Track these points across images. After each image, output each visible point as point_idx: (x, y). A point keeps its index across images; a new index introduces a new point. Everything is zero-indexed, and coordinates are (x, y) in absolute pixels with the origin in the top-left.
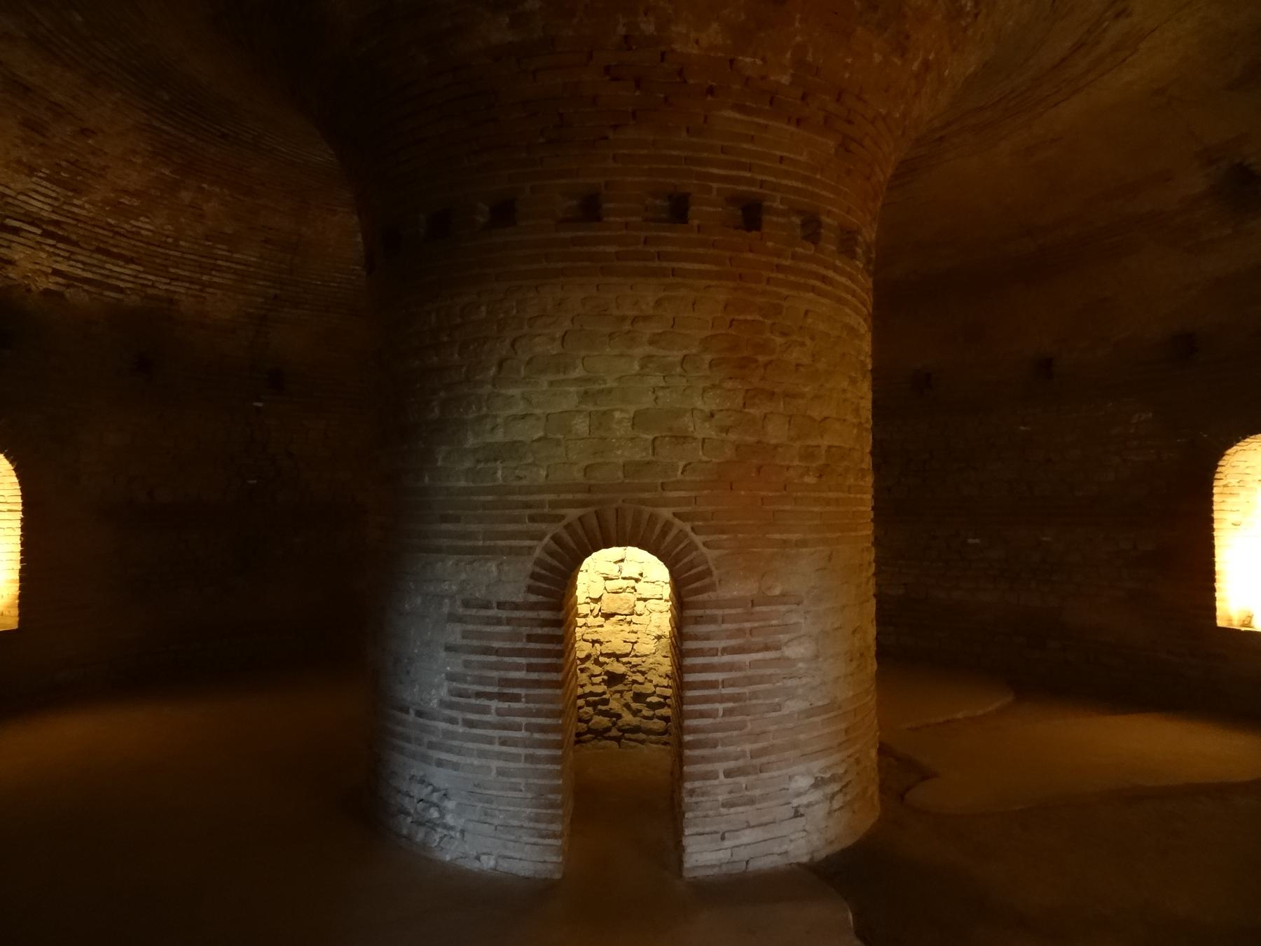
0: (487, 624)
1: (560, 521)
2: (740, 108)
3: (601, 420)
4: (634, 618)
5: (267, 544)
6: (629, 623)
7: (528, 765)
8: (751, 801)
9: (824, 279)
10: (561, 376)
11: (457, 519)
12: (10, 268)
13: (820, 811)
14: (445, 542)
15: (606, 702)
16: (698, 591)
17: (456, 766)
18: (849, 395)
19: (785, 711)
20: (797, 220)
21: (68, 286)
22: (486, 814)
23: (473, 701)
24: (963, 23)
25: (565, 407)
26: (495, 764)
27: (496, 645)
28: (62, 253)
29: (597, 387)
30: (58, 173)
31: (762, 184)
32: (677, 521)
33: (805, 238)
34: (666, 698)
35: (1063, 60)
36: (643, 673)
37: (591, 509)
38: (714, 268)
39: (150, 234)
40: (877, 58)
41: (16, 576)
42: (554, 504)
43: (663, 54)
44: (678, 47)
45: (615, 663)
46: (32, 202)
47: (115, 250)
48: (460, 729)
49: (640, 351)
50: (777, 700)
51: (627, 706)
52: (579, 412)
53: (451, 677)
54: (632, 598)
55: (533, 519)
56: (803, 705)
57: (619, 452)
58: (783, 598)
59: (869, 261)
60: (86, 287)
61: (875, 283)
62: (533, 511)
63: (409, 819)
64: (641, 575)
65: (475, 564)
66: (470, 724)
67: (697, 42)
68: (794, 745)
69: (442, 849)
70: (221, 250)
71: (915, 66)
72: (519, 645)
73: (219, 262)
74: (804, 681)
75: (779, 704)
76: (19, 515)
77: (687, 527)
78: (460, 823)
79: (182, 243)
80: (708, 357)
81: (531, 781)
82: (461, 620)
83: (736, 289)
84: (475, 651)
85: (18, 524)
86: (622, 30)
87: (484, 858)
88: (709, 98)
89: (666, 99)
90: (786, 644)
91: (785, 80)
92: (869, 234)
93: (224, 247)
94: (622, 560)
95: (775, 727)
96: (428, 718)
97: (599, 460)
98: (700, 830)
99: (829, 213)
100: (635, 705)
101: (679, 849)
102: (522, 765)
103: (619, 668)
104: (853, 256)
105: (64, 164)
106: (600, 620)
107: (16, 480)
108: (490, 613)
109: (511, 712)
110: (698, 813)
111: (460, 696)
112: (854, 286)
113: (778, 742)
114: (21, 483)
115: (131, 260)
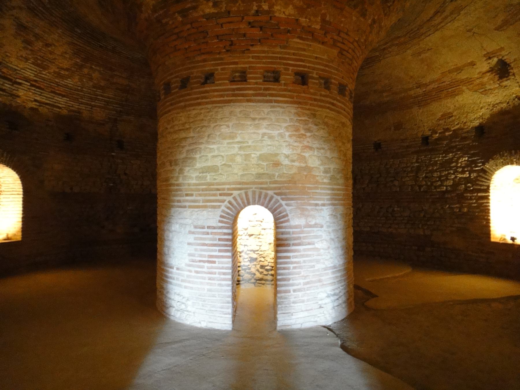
3: (247, 157)
5: (106, 229)
6: (259, 238)
8: (303, 301)
9: (333, 104)
10: (231, 141)
11: (192, 195)
12: (17, 98)
14: (187, 204)
15: (250, 269)
16: (282, 222)
17: (191, 288)
18: (342, 149)
20: (323, 81)
21: (40, 106)
22: (203, 306)
24: (389, 5)
25: (233, 153)
28: (38, 93)
29: (245, 145)
30: (36, 61)
31: (309, 67)
32: (275, 196)
33: (325, 88)
34: (273, 267)
35: (431, 18)
36: (264, 258)
38: (291, 100)
39: (72, 86)
40: (354, 18)
41: (21, 220)
42: (229, 189)
43: (271, 17)
44: (277, 14)
46: (26, 72)
47: (58, 92)
48: (193, 274)
49: (261, 131)
50: (313, 264)
51: (258, 270)
52: (238, 154)
53: (190, 255)
55: (221, 195)
56: (324, 266)
57: (253, 170)
58: (315, 225)
59: (351, 97)
60: (47, 106)
61: (354, 106)
62: (220, 192)
63: (174, 309)
65: (198, 212)
66: (197, 272)
67: (284, 13)
68: (320, 281)
69: (187, 320)
70: (99, 92)
71: (370, 21)
73: (99, 97)
74: (324, 257)
75: (314, 265)
76: (22, 196)
77: (279, 198)
79: (84, 89)
80: (287, 134)
81: (219, 293)
82: (193, 233)
83: (298, 108)
84: (199, 245)
85: (21, 200)
86: (255, 8)
87: (202, 322)
88: (289, 34)
89: (272, 35)
90: (317, 243)
91: (318, 27)
92: (351, 87)
96: (182, 271)
97: (246, 173)
98: (284, 312)
99: (335, 79)
100: (261, 270)
101: (275, 319)
103: (255, 256)
104: (344, 95)
105: (39, 57)
106: (248, 237)
107: (20, 182)
109: (212, 268)
110: (284, 306)
111: (193, 262)
112: (345, 107)
113: (313, 279)
114: (22, 183)
115: (63, 96)
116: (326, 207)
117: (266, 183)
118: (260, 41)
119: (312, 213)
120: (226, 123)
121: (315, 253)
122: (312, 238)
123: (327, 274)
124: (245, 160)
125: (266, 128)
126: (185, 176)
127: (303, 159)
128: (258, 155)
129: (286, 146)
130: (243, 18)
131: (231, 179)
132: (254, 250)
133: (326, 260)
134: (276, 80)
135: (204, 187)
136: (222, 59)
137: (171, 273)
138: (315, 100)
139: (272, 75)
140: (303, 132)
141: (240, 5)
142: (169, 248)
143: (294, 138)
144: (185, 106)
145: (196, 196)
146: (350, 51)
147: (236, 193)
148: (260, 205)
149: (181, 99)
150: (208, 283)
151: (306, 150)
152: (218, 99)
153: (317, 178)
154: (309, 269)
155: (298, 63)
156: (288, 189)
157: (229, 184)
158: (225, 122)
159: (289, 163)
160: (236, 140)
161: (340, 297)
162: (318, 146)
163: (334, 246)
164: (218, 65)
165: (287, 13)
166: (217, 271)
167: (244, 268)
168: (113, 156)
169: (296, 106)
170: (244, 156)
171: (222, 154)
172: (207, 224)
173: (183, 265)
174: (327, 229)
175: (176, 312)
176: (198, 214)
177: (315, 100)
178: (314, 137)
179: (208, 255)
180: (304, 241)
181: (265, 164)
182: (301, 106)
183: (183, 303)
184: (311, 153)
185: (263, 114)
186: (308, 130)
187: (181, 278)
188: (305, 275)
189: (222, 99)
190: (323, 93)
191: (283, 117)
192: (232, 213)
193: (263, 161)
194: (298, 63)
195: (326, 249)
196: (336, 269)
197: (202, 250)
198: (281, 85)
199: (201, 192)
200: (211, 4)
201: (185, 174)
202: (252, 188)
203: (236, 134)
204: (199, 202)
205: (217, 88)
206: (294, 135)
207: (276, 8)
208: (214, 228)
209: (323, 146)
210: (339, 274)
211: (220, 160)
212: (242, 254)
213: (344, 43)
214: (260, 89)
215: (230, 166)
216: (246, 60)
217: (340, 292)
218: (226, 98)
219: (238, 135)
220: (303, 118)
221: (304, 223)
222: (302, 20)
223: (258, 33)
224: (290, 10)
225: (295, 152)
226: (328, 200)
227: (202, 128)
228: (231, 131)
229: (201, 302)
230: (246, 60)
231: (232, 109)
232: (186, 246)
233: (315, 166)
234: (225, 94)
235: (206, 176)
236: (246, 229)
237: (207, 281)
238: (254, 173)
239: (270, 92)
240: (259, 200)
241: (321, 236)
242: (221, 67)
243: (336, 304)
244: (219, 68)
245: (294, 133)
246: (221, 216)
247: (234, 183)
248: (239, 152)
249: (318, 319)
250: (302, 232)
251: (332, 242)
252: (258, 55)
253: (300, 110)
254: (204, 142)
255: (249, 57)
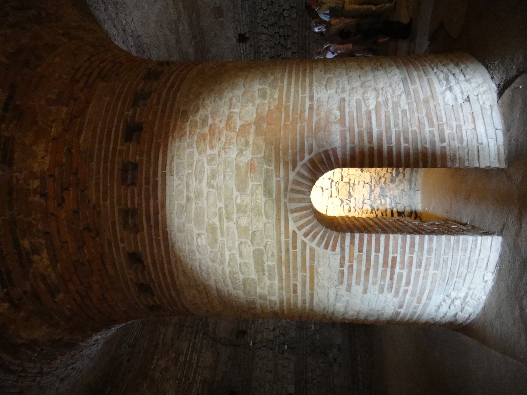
0: (352, 273)
1: (296, 234)
2: (80, 132)
3: (241, 209)
4: (352, 182)
6: (354, 184)
7: (433, 254)
9: (172, 86)
10: (219, 231)
11: (295, 286)
13: (465, 86)
17: (431, 291)
19: (406, 107)
22: (460, 277)
23: (395, 281)
25: (235, 229)
26: (431, 271)
27: (363, 268)
29: (224, 212)
31: (119, 122)
32: (297, 170)
37: (290, 216)
42: (287, 236)
45: (375, 192)
48: (410, 288)
50: (400, 113)
52: (237, 221)
53: (381, 291)
54: (341, 183)
55: (295, 247)
56: (403, 96)
57: (259, 201)
58: (342, 109)
63: (460, 313)
64: (329, 179)
65: (319, 278)
66: (408, 283)
67: (43, 158)
68: (426, 101)
70: (182, 359)
72: (364, 257)
73: (188, 359)
74: (389, 96)
75: (403, 111)
78: (464, 290)
80: (209, 152)
81: (442, 253)
83: (173, 137)
86: (37, 198)
87: (486, 279)
88: (73, 151)
90: (368, 107)
91: (65, 110)
93: (181, 358)
94: (322, 188)
95: (416, 113)
97: (263, 211)
98: (476, 156)
102: (433, 257)
103: (378, 190)
106: (352, 200)
108: (346, 272)
109: (402, 262)
111: (392, 288)
116: (315, 94)
117: (278, 182)
118: (83, 191)
119: (322, 115)
120: (195, 237)
121: (383, 110)
122: (361, 114)
123: (415, 91)
124: (246, 212)
125: (201, 182)
126: (269, 293)
127: (244, 128)
128: (238, 193)
129: (226, 153)
130: (52, 214)
131: (272, 232)
132: (369, 191)
133: (394, 92)
134: (135, 166)
135: (283, 269)
136: (109, 242)
137: (405, 315)
138: (163, 112)
139: (130, 172)
140: (206, 130)
141: (34, 219)
142: (367, 315)
143: (215, 141)
144: (176, 290)
145: (297, 281)
146: (102, 65)
147: (292, 226)
148: (310, 192)
149: (166, 293)
150: (426, 269)
151: (232, 125)
152: (163, 248)
153: (273, 107)
154: (409, 119)
155: (112, 138)
156: (288, 151)
157: (279, 235)
158: (193, 238)
159: (250, 149)
160: (218, 223)
161: (450, 72)
162: (226, 107)
163: (373, 82)
164: (117, 247)
165: (43, 154)
166: (407, 255)
167: (393, 205)
168: (254, 343)
169: (170, 139)
170: (240, 215)
171: (237, 244)
172: (338, 268)
173: (396, 300)
174: (348, 93)
175: (464, 311)
176: (323, 279)
177: (163, 112)
178: (214, 114)
179: (383, 267)
180: (364, 126)
181: (251, 184)
182: (170, 133)
183: (453, 302)
184: (236, 117)
185: (181, 186)
186: (204, 121)
187: (415, 304)
188: (417, 124)
189: (162, 243)
190: (154, 102)
191: (186, 158)
192: (321, 233)
193: (246, 186)
194: (112, 138)
195: (378, 94)
196: (408, 79)
197: (375, 275)
198: (142, 161)
199: (291, 274)
200: (36, 258)
201: (266, 293)
202: (285, 202)
203: (209, 224)
204: (305, 277)
205: (148, 249)
206: (211, 141)
207: (36, 168)
208: (343, 258)
209: (227, 100)
210: (415, 74)
211: (245, 247)
212: (375, 206)
213: (91, 74)
214: (147, 190)
215: (254, 233)
216: (109, 210)
217: (442, 71)
218: (161, 238)
219: (211, 222)
220: (188, 129)
221: (338, 126)
222: (53, 131)
223: (71, 193)
224: (40, 149)
225: (234, 141)
226: (304, 91)
227: (203, 271)
228: (204, 231)
229: (455, 280)
230: (109, 210)
231: (176, 230)
232: (368, 296)
233: (255, 111)
234: (156, 239)
235: (268, 266)
236: (342, 201)
237: (422, 270)
238: (264, 200)
239: (151, 175)
240: (303, 193)
241: (358, 102)
242: (120, 242)
243: (462, 78)
244: (121, 245)
245: (208, 141)
246: (326, 247)
247: (278, 229)
248: (235, 220)
249: (488, 104)
250: (352, 129)
251: (367, 84)
252: (101, 194)
253: (175, 135)
254: (221, 268)
255: (105, 206)
